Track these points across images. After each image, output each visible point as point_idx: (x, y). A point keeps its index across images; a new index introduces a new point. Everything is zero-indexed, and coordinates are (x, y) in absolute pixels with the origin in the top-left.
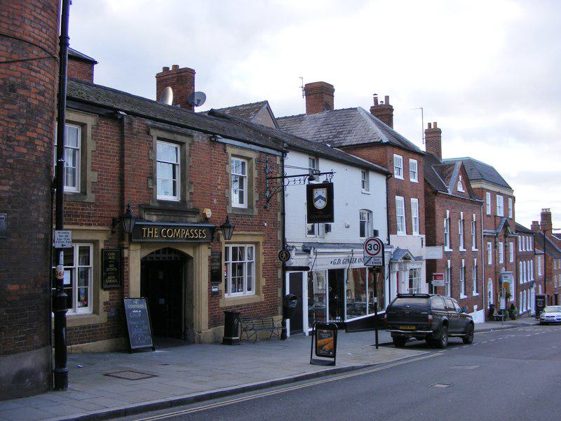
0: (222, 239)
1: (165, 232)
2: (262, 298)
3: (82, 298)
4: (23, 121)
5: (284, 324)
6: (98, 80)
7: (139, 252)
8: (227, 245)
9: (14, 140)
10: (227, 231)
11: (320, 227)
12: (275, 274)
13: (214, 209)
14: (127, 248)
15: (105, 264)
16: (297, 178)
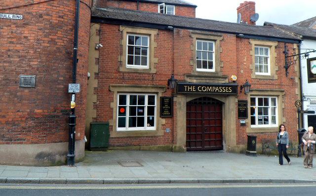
1: (200, 89)
4: (47, 31)
9: (41, 40)
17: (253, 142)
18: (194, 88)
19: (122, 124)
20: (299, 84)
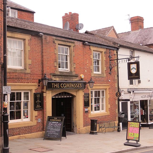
0: (89, 87)
2: (108, 113)
3: (26, 114)
5: (119, 125)
6: (36, 20)
7: (51, 94)
8: (92, 89)
10: (91, 84)
11: (135, 81)
12: (115, 103)
13: (85, 75)
14: (45, 92)
15: (35, 98)
16: (123, 60)
18: (58, 85)
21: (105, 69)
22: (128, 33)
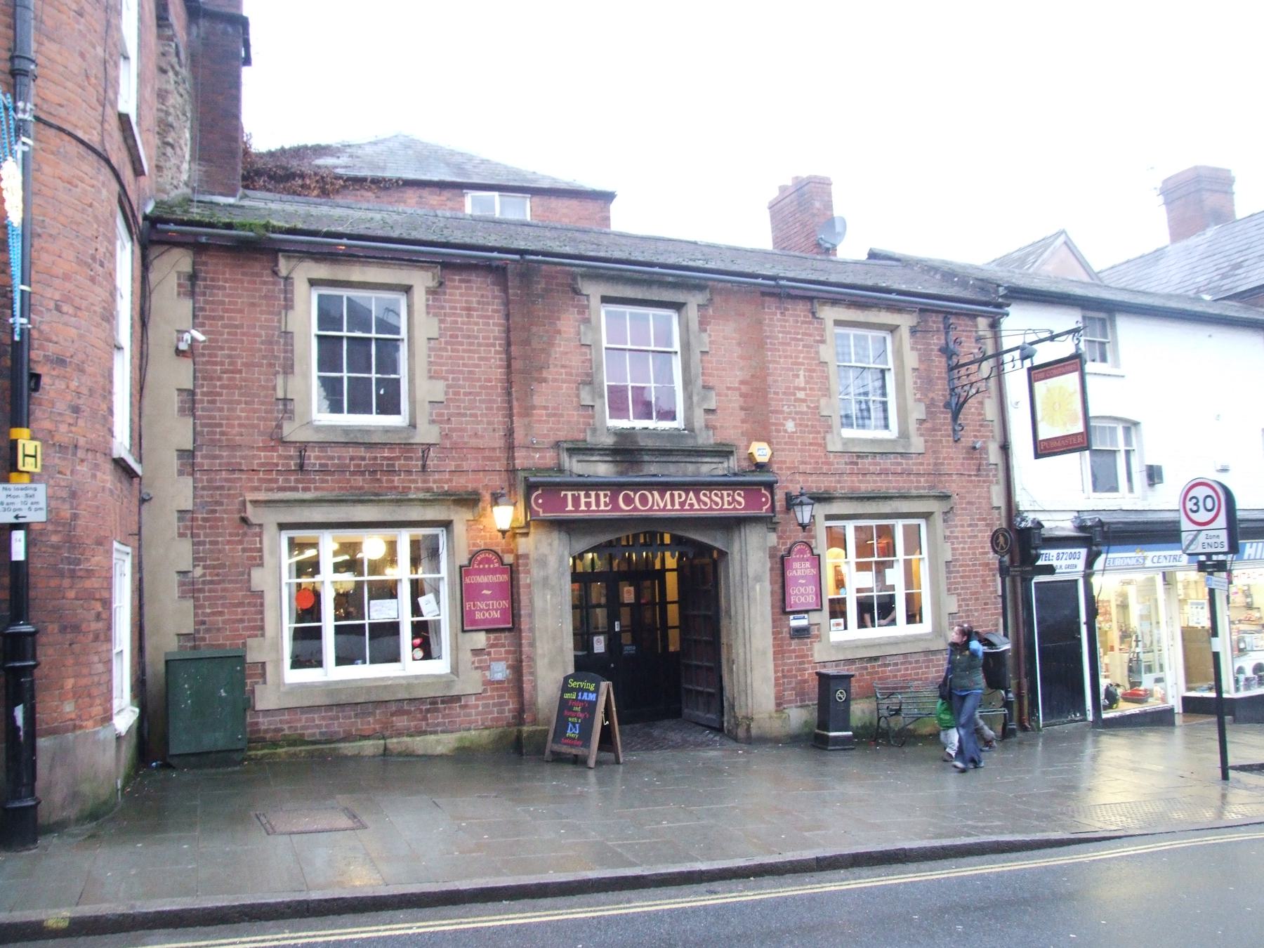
17: (840, 695)
18: (602, 499)
19: (307, 657)
20: (1001, 467)
21: (917, 412)
22: (1158, 254)
